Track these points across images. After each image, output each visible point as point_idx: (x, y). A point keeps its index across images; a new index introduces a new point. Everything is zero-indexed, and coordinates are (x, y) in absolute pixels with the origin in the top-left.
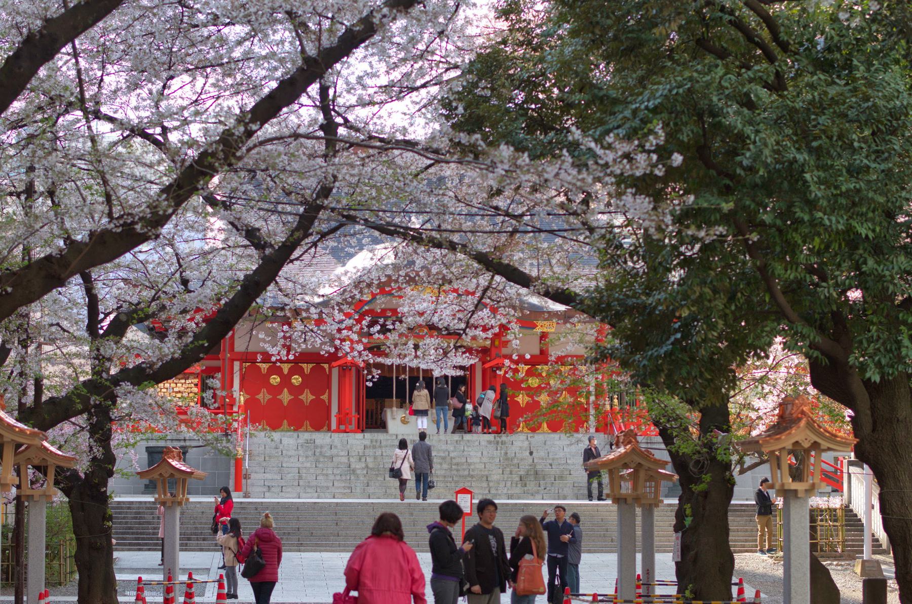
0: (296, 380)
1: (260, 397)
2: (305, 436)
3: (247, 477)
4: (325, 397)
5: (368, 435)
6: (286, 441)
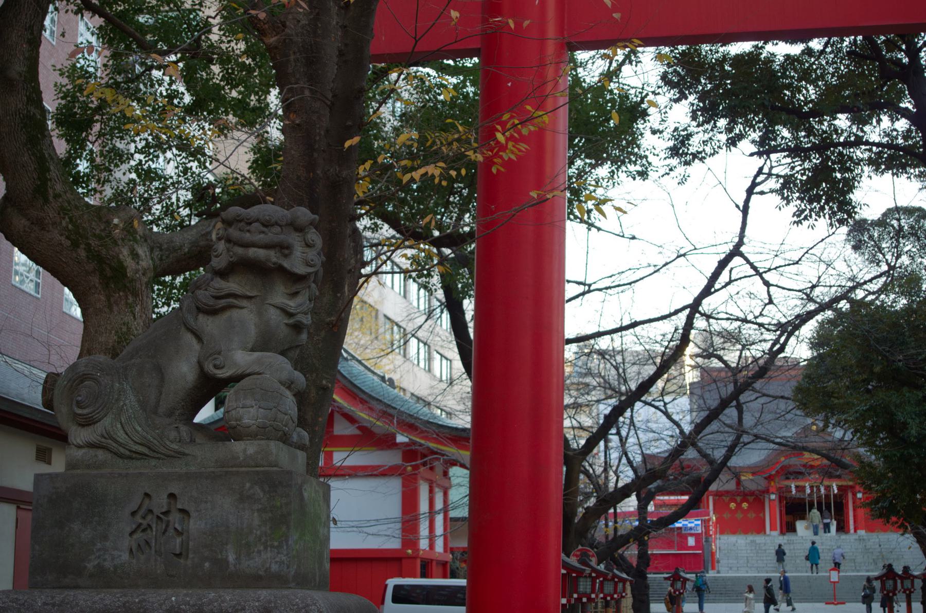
0: (745, 505)
1: (725, 516)
2: (750, 538)
3: (718, 562)
4: (761, 515)
5: (785, 537)
6: (739, 541)
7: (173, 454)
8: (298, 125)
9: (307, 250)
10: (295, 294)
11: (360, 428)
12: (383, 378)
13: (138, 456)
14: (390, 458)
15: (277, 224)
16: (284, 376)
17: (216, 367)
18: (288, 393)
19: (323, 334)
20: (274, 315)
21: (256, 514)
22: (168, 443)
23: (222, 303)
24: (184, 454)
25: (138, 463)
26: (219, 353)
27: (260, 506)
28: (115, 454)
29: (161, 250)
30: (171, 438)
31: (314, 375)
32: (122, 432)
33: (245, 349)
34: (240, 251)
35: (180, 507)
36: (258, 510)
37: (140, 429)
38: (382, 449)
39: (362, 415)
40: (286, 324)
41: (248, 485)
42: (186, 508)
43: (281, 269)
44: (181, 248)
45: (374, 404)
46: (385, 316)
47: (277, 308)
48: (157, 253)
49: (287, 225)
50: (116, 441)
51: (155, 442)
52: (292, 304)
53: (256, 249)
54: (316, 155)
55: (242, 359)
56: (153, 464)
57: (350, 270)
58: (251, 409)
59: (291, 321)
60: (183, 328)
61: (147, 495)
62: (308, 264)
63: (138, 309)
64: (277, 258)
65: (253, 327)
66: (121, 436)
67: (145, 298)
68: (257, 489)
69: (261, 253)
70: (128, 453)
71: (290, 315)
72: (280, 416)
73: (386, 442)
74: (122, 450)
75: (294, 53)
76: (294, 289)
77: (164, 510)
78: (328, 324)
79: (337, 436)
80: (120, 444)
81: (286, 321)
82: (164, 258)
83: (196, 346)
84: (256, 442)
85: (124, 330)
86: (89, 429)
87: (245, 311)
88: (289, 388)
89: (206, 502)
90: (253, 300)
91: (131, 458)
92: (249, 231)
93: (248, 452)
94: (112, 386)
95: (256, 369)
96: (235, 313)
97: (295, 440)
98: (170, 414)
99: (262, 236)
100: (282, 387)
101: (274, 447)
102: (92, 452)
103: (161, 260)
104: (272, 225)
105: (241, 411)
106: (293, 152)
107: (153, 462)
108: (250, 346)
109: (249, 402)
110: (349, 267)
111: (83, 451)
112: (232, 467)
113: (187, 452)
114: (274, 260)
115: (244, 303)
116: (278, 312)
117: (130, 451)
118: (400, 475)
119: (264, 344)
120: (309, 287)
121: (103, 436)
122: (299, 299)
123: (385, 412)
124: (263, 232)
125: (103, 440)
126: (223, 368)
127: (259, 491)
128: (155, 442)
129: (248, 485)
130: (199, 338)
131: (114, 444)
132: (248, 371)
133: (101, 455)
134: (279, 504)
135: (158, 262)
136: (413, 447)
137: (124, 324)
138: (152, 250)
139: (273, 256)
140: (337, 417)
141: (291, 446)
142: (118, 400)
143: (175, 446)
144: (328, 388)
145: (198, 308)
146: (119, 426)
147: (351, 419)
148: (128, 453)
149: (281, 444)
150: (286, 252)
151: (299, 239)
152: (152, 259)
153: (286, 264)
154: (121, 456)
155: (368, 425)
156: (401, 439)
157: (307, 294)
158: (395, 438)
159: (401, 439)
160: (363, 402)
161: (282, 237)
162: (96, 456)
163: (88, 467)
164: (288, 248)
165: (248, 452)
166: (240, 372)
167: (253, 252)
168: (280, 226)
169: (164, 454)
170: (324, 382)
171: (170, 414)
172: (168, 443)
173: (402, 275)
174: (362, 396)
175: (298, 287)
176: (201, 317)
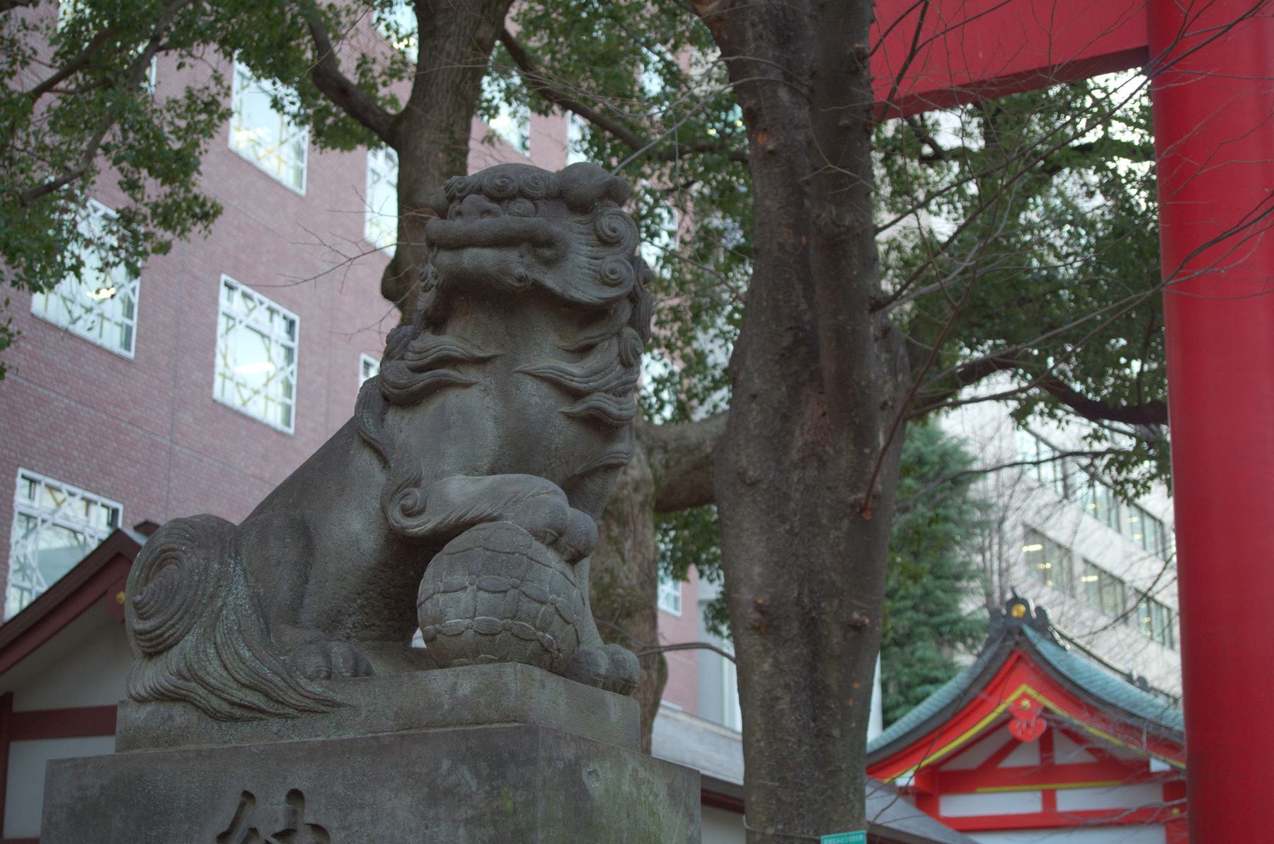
7: (312, 704)
8: (771, 152)
9: (603, 251)
10: (584, 351)
11: (1092, 751)
12: (1129, 678)
13: (247, 714)
14: (1148, 796)
15: (522, 194)
16: (541, 518)
17: (408, 513)
18: (551, 556)
19: (845, 524)
20: (535, 396)
21: (462, 832)
22: (303, 681)
23: (426, 378)
24: (335, 704)
25: (247, 729)
26: (417, 483)
27: (470, 813)
28: (205, 711)
29: (666, 451)
30: (310, 670)
31: (836, 603)
32: (216, 663)
33: (473, 471)
34: (445, 258)
35: (310, 819)
36: (467, 822)
37: (247, 654)
38: (1128, 783)
39: (1093, 730)
40: (568, 416)
41: (446, 764)
42: (323, 822)
43: (540, 296)
44: (699, 446)
45: (1109, 713)
46: (1086, 561)
47: (533, 376)
48: (659, 457)
49: (548, 197)
50: (203, 683)
51: (277, 680)
52: (576, 371)
53: (475, 250)
54: (807, 203)
55: (460, 490)
56: (275, 729)
57: (885, 404)
58: (461, 594)
59: (578, 408)
60: (356, 443)
61: (248, 795)
62: (606, 282)
63: (628, 544)
64: (528, 267)
65: (490, 424)
66: (214, 671)
67: (640, 528)
68: (465, 773)
69: (486, 258)
70: (226, 707)
71: (576, 395)
72: (528, 606)
73: (1134, 772)
74: (215, 702)
75: (753, 25)
76: (582, 338)
77: (279, 828)
78: (853, 506)
79: (244, 523)
80: (212, 690)
81: (566, 409)
82: (672, 463)
83: (379, 476)
84: (476, 669)
85: (607, 579)
86: (160, 662)
87: (475, 391)
88: (554, 544)
89: (362, 807)
90: (489, 367)
91: (231, 718)
92: (459, 214)
93: (460, 693)
94: (206, 569)
95: (484, 508)
96: (453, 398)
97: (603, 671)
98: (331, 624)
99: (487, 220)
100: (536, 544)
101: (513, 675)
102: (163, 709)
103: (667, 466)
104: (512, 198)
105: (441, 598)
106: (768, 203)
107: (275, 724)
108: (485, 463)
109: (459, 578)
110: (882, 399)
111: (149, 708)
112: (427, 726)
113: (339, 698)
114: (521, 270)
115: (471, 374)
116: (545, 389)
117: (232, 704)
118: (1156, 821)
119: (520, 454)
120: (619, 334)
121: (180, 675)
122: (593, 362)
123: (1126, 726)
124: (488, 212)
125: (181, 683)
126: (420, 512)
127: (468, 776)
128: (277, 680)
129: (446, 764)
130: (384, 460)
131: (201, 691)
132: (469, 516)
133: (181, 715)
134: (509, 805)
135: (661, 471)
136: (1175, 778)
137: (606, 570)
138: (650, 451)
139: (516, 264)
140: (1058, 739)
141: (595, 684)
142: (213, 597)
143: (316, 688)
144: (864, 625)
145: (386, 398)
146: (212, 651)
147: (1076, 737)
148: (226, 707)
149: (538, 673)
150: (547, 253)
151: (582, 228)
152: (651, 466)
153: (551, 281)
154: (215, 716)
155: (1102, 746)
156: (1157, 765)
157: (615, 350)
158: (1147, 764)
159: (1157, 765)
160: (1092, 711)
161: (532, 221)
162: (171, 717)
163: (156, 742)
164: (549, 243)
165: (460, 693)
166: (454, 517)
167: (473, 258)
168: (532, 199)
169: (296, 708)
170: (856, 615)
171: (331, 624)
172: (303, 681)
173: (1058, 462)
174: (1091, 701)
175: (592, 333)
176: (392, 417)
